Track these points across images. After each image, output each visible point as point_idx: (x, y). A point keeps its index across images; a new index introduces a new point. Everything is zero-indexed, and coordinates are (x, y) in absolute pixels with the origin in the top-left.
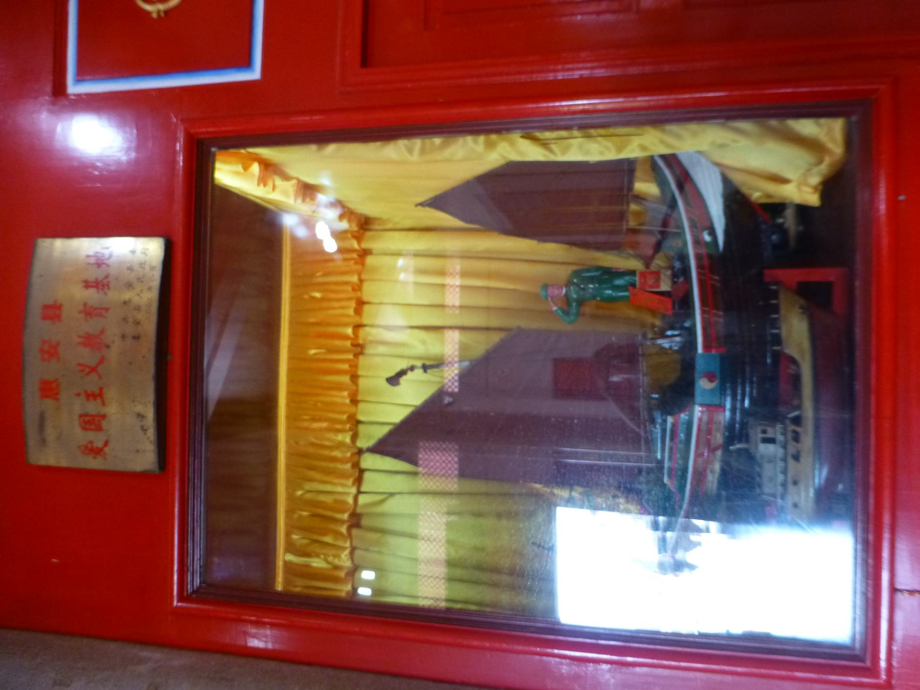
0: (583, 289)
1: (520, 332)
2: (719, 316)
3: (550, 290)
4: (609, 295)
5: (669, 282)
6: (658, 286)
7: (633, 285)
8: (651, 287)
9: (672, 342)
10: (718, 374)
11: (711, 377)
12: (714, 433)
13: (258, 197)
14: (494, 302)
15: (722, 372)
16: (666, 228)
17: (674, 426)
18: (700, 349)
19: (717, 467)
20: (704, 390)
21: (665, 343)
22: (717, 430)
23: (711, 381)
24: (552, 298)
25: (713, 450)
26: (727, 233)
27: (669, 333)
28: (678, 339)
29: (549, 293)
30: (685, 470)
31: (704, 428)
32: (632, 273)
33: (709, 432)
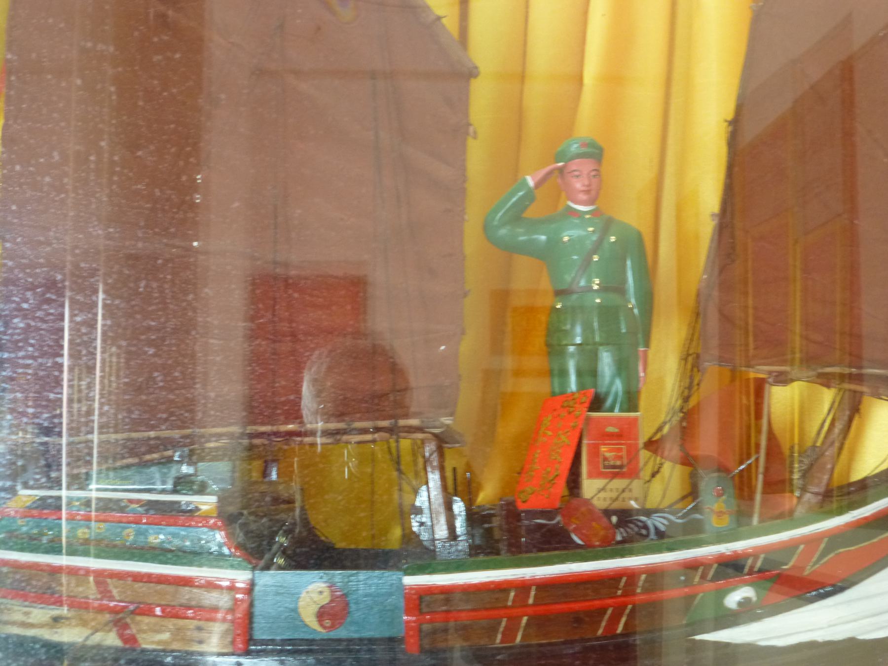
0: (588, 261)
1: (467, 74)
2: (510, 633)
3: (585, 167)
4: (568, 334)
5: (600, 503)
6: (595, 474)
7: (597, 403)
8: (595, 452)
9: (432, 511)
10: (342, 633)
11: (334, 611)
12: (171, 623)
13: (769, 407)
14: (544, 54)
15: (349, 646)
16: (762, 472)
17: (189, 515)
18: (410, 581)
19: (70, 635)
20: (296, 596)
21: (429, 493)
22: (178, 633)
23: (322, 614)
24: (561, 170)
25: (120, 620)
26: (752, 651)
27: (459, 507)
28: (442, 532)
29: (574, 165)
30: (54, 548)
31: (186, 594)
32: (631, 401)
33: (173, 613)
